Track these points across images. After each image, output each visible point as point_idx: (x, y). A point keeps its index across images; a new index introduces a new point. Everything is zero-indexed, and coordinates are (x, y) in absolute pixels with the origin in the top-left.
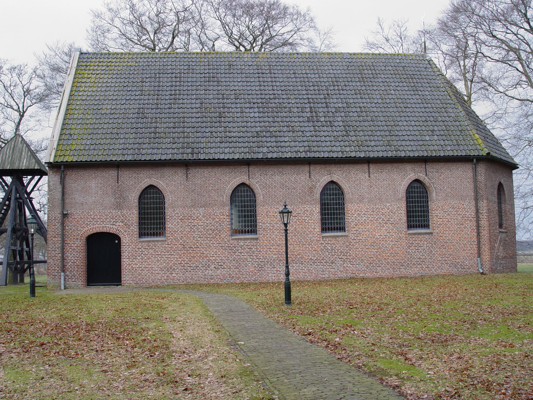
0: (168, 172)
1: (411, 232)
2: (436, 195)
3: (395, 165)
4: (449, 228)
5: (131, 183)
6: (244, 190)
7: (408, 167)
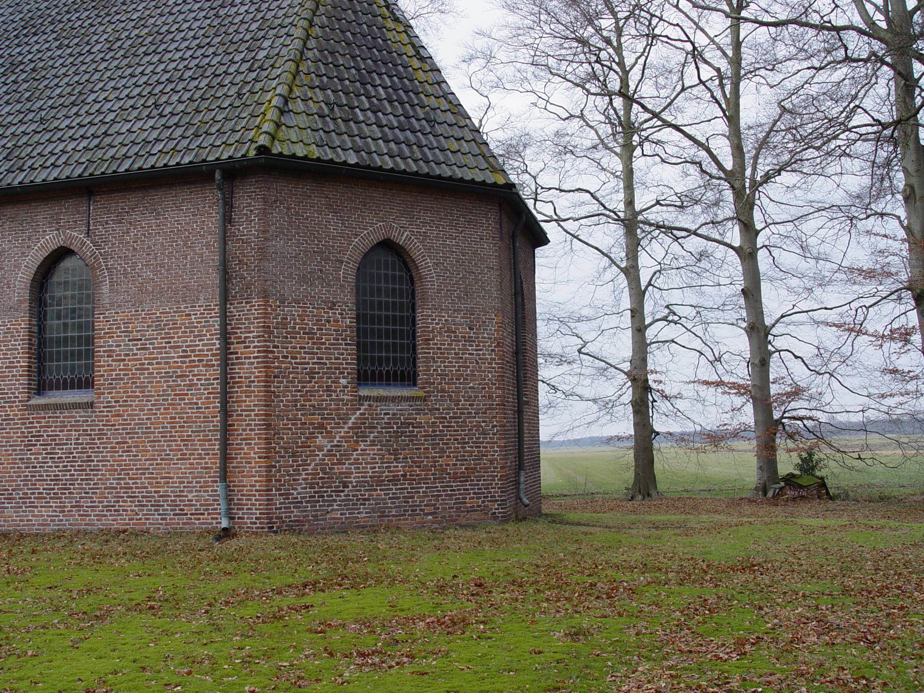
1: (364, 392)
2: (111, 291)
4: (143, 388)
6: (386, 263)
7: (42, 213)
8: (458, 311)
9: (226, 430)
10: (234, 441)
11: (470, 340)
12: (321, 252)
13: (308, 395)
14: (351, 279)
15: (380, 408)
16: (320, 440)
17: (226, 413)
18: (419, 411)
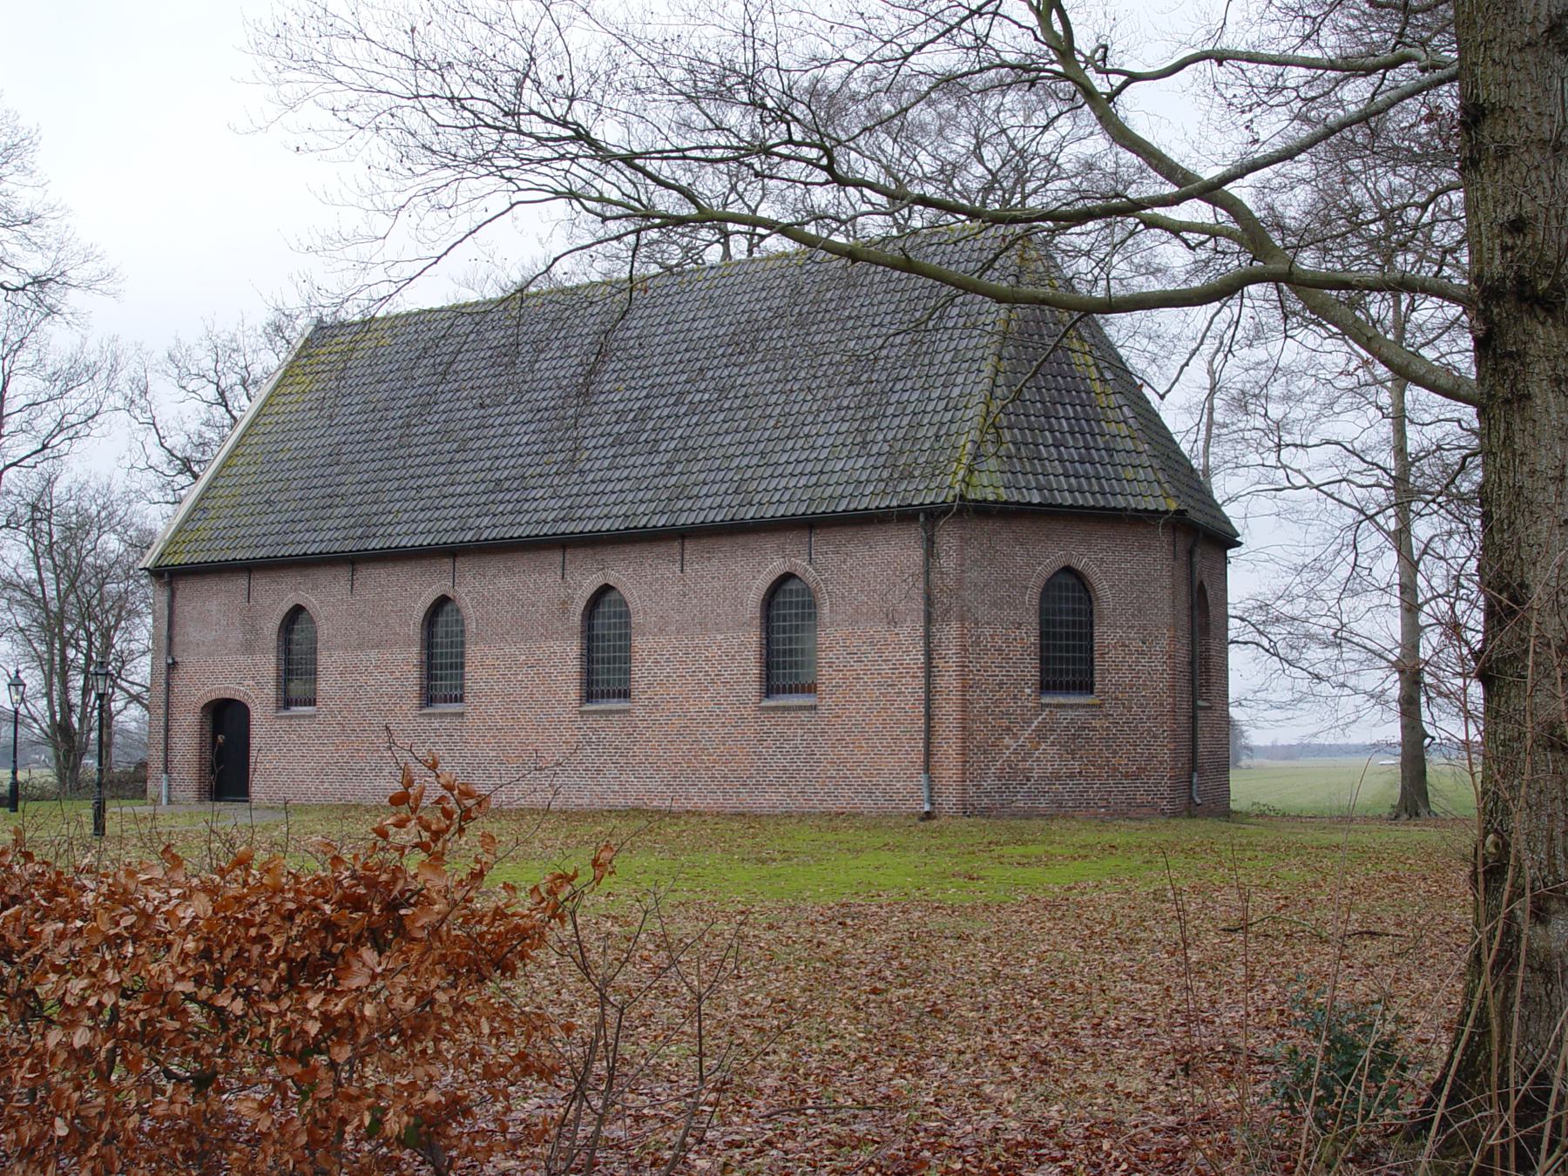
0: (323, 576)
1: (1046, 700)
3: (741, 540)
4: (858, 694)
5: (269, 601)
7: (769, 543)
8: (1132, 627)
9: (929, 731)
10: (936, 740)
11: (1143, 653)
13: (997, 703)
14: (1036, 602)
15: (1060, 714)
16: (1007, 741)
17: (929, 716)
18: (1094, 717)
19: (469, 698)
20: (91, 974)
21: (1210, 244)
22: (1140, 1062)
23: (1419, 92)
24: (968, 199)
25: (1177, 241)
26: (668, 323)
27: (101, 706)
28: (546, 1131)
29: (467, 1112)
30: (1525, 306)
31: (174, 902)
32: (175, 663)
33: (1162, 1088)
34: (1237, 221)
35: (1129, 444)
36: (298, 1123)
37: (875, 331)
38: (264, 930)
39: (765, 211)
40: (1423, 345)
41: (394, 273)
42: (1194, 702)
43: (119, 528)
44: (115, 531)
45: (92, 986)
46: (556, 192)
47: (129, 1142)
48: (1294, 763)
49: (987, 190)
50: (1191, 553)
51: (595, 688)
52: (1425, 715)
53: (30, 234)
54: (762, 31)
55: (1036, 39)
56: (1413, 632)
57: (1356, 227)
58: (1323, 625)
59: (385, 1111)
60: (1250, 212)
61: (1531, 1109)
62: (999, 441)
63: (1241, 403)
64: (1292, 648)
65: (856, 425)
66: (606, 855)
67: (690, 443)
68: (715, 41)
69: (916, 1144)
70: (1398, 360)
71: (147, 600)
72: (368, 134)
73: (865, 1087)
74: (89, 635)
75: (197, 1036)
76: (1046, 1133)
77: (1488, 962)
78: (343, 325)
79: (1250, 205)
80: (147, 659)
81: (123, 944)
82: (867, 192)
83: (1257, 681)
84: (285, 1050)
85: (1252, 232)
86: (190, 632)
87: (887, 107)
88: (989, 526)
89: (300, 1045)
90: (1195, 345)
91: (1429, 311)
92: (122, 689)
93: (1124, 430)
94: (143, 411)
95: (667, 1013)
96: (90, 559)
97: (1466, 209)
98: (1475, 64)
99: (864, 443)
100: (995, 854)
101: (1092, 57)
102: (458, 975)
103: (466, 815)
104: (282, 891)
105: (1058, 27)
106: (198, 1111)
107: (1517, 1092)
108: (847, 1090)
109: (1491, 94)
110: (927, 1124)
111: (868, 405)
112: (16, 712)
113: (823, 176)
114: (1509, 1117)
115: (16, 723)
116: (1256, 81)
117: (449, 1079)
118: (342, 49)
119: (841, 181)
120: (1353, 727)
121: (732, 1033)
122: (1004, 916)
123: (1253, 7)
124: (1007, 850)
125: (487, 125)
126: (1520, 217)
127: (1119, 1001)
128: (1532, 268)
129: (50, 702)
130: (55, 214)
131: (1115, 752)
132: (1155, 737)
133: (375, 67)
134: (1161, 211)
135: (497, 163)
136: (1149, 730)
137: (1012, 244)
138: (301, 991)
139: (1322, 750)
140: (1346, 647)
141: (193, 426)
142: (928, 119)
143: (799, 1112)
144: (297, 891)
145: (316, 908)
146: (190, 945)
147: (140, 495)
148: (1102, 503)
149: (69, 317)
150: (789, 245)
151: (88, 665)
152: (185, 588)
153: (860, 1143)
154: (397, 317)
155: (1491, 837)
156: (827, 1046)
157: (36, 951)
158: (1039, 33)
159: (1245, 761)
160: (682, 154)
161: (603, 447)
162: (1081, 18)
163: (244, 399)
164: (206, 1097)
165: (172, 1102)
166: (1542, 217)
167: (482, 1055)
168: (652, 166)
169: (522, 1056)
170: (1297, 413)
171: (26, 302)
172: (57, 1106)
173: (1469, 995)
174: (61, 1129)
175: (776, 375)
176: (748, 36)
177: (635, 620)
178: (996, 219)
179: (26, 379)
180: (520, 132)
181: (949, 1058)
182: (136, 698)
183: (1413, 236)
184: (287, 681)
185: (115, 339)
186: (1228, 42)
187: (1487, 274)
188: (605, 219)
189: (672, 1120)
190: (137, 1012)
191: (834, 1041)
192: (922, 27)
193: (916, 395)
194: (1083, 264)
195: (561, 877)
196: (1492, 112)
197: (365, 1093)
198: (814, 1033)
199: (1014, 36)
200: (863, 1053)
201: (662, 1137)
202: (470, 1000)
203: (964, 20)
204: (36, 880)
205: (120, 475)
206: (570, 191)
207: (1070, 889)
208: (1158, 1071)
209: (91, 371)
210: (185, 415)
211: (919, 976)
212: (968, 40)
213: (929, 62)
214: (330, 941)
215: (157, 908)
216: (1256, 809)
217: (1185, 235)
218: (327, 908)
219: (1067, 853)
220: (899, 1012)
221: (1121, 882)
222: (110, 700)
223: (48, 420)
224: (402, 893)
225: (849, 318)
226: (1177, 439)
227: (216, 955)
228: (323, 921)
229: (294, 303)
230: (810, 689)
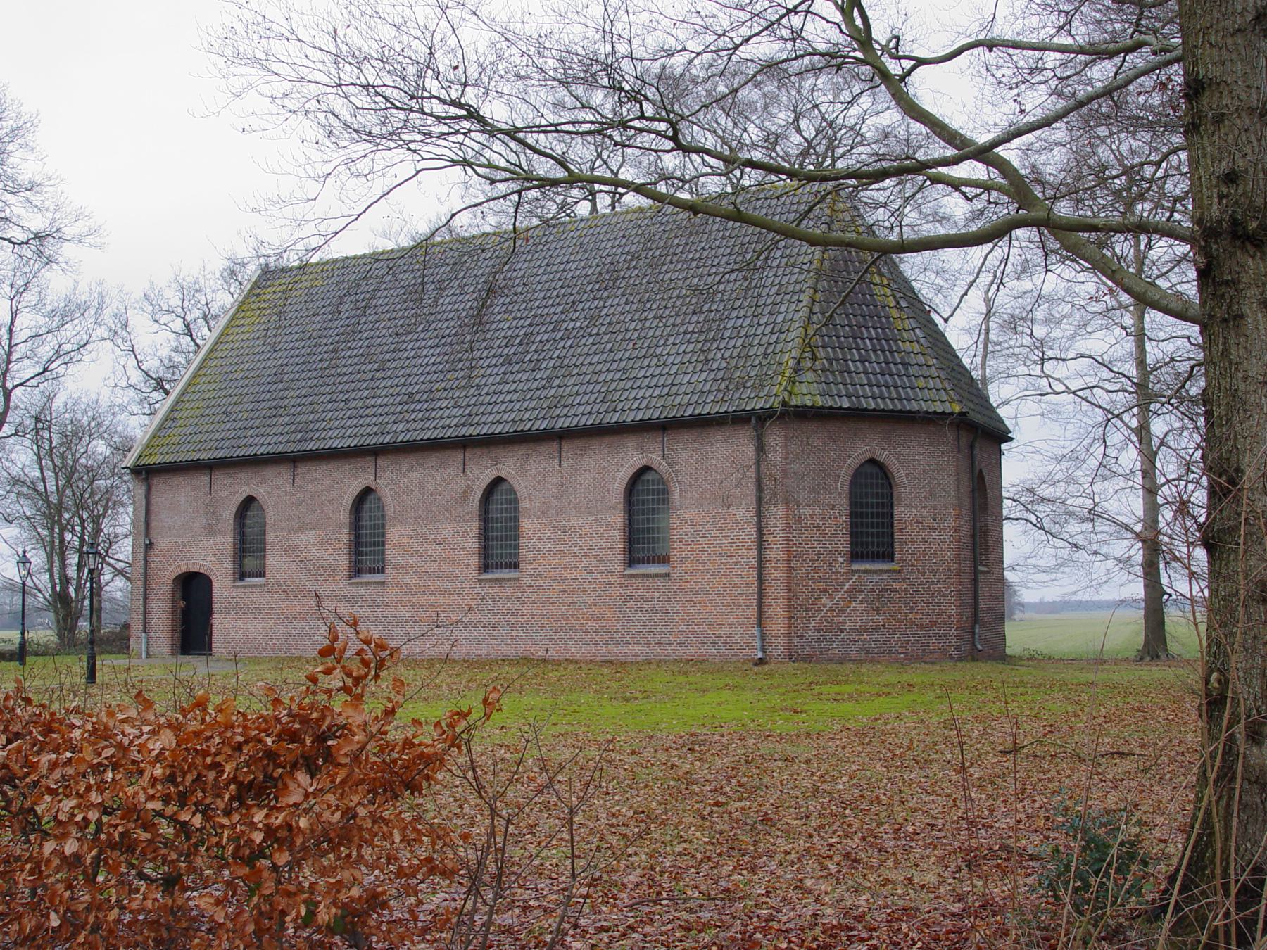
1: (855, 567)
3: (607, 440)
7: (631, 442)
8: (925, 507)
9: (761, 593)
10: (766, 601)
11: (933, 528)
12: (824, 471)
13: (816, 569)
14: (846, 487)
15: (867, 578)
16: (824, 600)
17: (761, 581)
18: (895, 580)
19: (389, 570)
20: (79, 795)
21: (984, 197)
22: (933, 859)
23: (1153, 70)
24: (789, 162)
25: (956, 194)
26: (547, 265)
27: (92, 579)
28: (448, 920)
29: (384, 905)
30: (1238, 243)
31: (145, 737)
32: (151, 544)
33: (951, 880)
34: (1005, 177)
35: (921, 359)
36: (246, 915)
37: (714, 270)
38: (218, 759)
39: (625, 175)
40: (1158, 277)
41: (323, 228)
42: (975, 567)
43: (106, 435)
44: (103, 438)
45: (79, 806)
46: (453, 161)
47: (111, 932)
48: (1057, 616)
49: (804, 154)
50: (972, 447)
51: (490, 561)
52: (1164, 580)
53: (32, 198)
54: (618, 27)
55: (841, 31)
56: (1152, 509)
57: (1103, 181)
58: (1080, 503)
59: (317, 904)
60: (1016, 170)
61: (1249, 895)
62: (814, 358)
63: (1012, 325)
64: (1055, 523)
65: (699, 345)
66: (495, 695)
67: (566, 362)
68: (580, 36)
69: (750, 928)
70: (1137, 289)
71: (129, 494)
72: (300, 118)
73: (709, 881)
74: (83, 522)
75: (165, 845)
76: (855, 918)
77: (1212, 776)
78: (284, 270)
79: (1016, 164)
80: (129, 541)
81: (104, 771)
82: (707, 158)
83: (1028, 549)
84: (234, 856)
85: (1017, 187)
86: (164, 519)
87: (721, 88)
88: (809, 427)
89: (248, 852)
90: (972, 278)
91: (1162, 249)
92: (109, 565)
93: (917, 348)
94: (124, 340)
95: (549, 823)
96: (83, 461)
97: (1190, 166)
98: (1196, 47)
99: (707, 360)
100: (815, 692)
101: (887, 45)
102: (376, 794)
103: (381, 664)
104: (232, 726)
105: (858, 22)
106: (166, 905)
107: (1237, 881)
108: (695, 885)
109: (1208, 71)
110: (759, 912)
111: (709, 330)
112: (24, 584)
113: (669, 145)
114: (1230, 903)
115: (24, 592)
116: (1021, 63)
117: (372, 878)
118: (278, 47)
119: (686, 149)
120: (1105, 587)
121: (601, 839)
122: (822, 742)
123: (1017, 4)
124: (825, 689)
125: (397, 108)
126: (1233, 170)
127: (915, 810)
128: (1244, 212)
129: (52, 576)
130: (52, 182)
131: (912, 608)
132: (944, 596)
133: (306, 62)
134: (944, 170)
135: (404, 137)
136: (939, 591)
137: (823, 199)
138: (249, 807)
139: (1080, 605)
140: (1098, 522)
141: (165, 352)
142: (755, 97)
143: (656, 903)
144: (245, 727)
145: (260, 741)
146: (158, 771)
147: (123, 408)
148: (899, 407)
149: (64, 265)
150: (644, 202)
151: (81, 546)
152: (159, 483)
153: (704, 927)
154: (327, 262)
155: (1215, 675)
156: (678, 849)
157: (34, 777)
158: (843, 27)
159: (1018, 615)
160: (556, 128)
161: (495, 365)
162: (878, 14)
163: (205, 331)
164: (172, 894)
165: (145, 899)
166: (1251, 170)
167: (396, 859)
168: (530, 139)
169: (429, 860)
170: (1056, 333)
171: (29, 254)
172: (51, 902)
173: (1198, 800)
174: (55, 921)
175: (635, 307)
176: (608, 34)
177: (522, 505)
178: (811, 178)
179: (30, 316)
180: (423, 113)
181: (777, 857)
182: (121, 572)
183: (1149, 189)
184: (242, 557)
185: (100, 283)
186: (996, 32)
187: (1207, 217)
188: (493, 182)
189: (553, 910)
190: (117, 825)
191: (685, 845)
192: (748, 24)
193: (748, 321)
194: (881, 214)
195: (457, 713)
196: (1210, 85)
197: (301, 889)
198: (668, 838)
199: (824, 31)
200: (708, 854)
201: (544, 924)
202: (386, 814)
203: (782, 17)
204: (35, 720)
205: (106, 392)
206: (465, 159)
207: (876, 720)
208: (947, 867)
209: (83, 308)
210: (158, 343)
211: (754, 790)
212: (786, 33)
213: (754, 51)
214: (271, 767)
215: (131, 742)
216: (1026, 654)
217: (963, 189)
218: (269, 741)
219: (876, 689)
220: (737, 820)
221: (917, 713)
222: (100, 574)
223: (47, 348)
224: (329, 728)
225: (693, 259)
226: (960, 355)
227: (179, 779)
228: (265, 751)
229: (244, 252)
230: (665, 560)
